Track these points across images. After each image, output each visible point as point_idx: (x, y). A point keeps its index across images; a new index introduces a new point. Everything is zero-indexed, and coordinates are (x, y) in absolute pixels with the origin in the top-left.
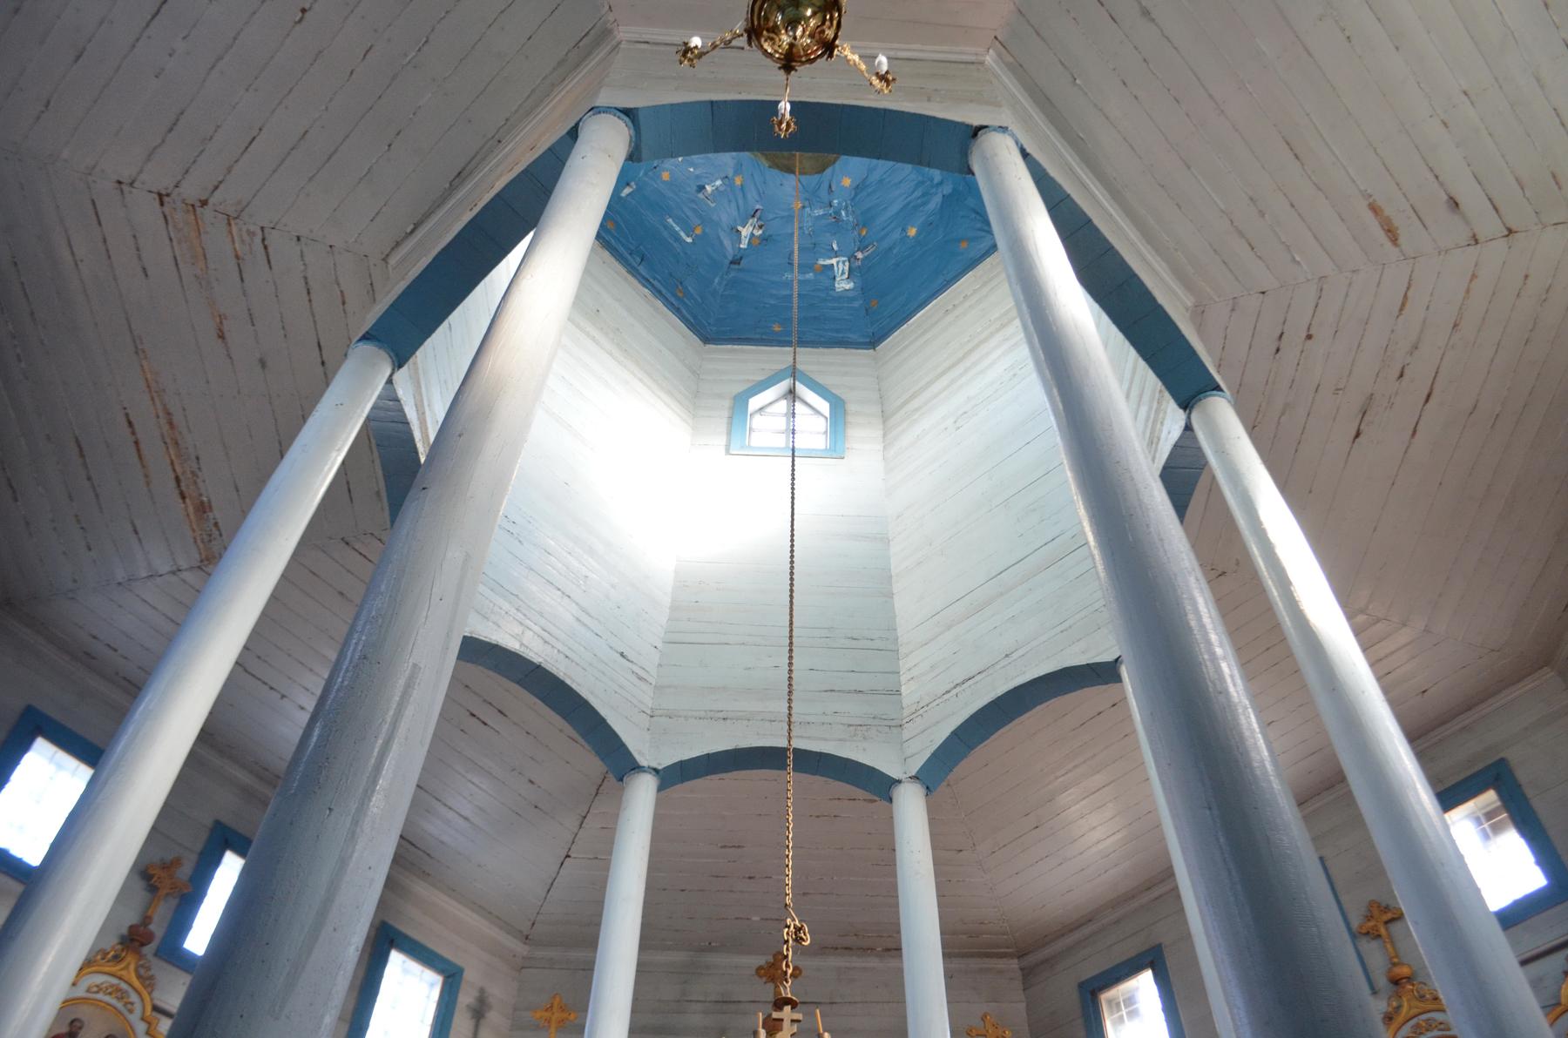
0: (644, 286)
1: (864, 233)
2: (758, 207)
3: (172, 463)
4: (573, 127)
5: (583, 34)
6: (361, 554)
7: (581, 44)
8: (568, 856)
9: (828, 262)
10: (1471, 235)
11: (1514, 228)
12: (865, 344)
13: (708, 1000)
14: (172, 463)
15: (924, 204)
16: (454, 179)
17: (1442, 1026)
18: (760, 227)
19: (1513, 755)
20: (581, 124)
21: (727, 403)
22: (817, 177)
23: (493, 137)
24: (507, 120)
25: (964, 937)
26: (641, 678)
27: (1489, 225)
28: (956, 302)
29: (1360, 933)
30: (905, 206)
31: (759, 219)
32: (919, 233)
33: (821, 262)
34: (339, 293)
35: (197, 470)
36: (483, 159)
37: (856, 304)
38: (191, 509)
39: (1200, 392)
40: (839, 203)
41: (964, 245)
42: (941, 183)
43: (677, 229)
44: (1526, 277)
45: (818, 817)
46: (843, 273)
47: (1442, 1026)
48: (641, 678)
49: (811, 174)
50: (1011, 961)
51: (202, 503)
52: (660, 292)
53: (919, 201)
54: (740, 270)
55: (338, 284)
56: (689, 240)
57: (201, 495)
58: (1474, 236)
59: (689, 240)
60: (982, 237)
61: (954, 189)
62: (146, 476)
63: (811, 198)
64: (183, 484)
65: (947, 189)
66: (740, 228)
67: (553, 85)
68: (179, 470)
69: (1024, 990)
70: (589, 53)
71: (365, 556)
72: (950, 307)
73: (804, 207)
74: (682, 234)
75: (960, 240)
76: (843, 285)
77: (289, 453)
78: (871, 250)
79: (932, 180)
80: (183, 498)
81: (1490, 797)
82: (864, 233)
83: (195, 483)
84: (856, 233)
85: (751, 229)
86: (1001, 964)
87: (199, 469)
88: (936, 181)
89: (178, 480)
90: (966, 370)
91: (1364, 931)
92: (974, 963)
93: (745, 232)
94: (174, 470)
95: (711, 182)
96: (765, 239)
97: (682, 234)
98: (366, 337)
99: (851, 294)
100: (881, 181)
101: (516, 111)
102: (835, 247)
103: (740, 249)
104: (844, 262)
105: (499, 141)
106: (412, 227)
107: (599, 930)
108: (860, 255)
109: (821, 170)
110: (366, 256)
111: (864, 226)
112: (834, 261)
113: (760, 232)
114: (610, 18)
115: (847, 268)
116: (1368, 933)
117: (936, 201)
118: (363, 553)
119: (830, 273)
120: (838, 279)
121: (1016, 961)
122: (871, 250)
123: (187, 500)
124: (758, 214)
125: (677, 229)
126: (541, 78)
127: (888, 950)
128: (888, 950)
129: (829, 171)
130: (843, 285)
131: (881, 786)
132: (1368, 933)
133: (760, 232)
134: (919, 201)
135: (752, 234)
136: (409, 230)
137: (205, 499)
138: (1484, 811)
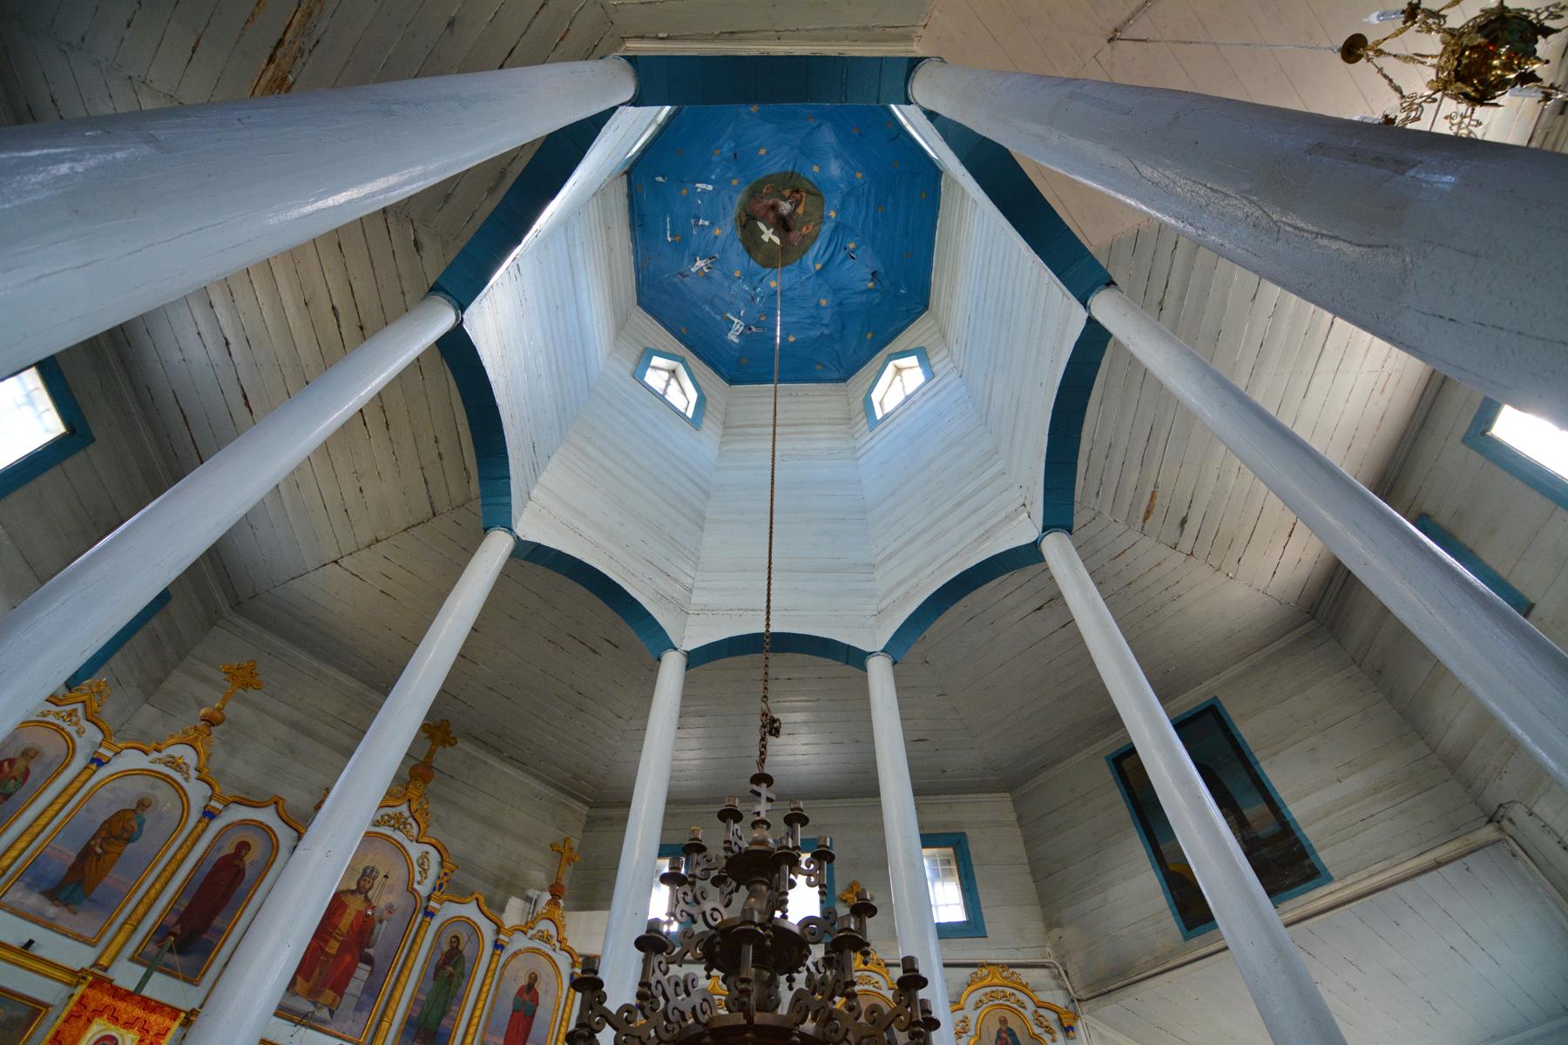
0: (632, 241)
2: (717, 255)
3: (289, 26)
4: (917, 58)
7: (888, 29)
8: (336, 562)
10: (1176, 542)
11: (1194, 554)
12: (726, 378)
13: (359, 727)
14: (289, 26)
15: (808, 329)
16: (724, 33)
17: (877, 985)
18: (709, 268)
19: (971, 834)
20: (927, 60)
21: (641, 348)
22: (760, 268)
23: (777, 31)
24: (798, 30)
25: (568, 775)
26: (534, 470)
27: (1186, 545)
28: (800, 394)
29: (841, 899)
31: (712, 263)
32: (794, 342)
33: (729, 315)
34: (565, 29)
36: (758, 39)
37: (733, 353)
41: (819, 367)
42: (826, 325)
43: (668, 227)
44: (1178, 582)
46: (737, 331)
47: (877, 985)
48: (534, 470)
49: (758, 263)
51: (285, 79)
52: (637, 253)
53: (807, 326)
55: (571, 23)
56: (669, 239)
57: (290, 72)
58: (1176, 544)
59: (669, 239)
60: (832, 370)
62: (253, 15)
63: (748, 276)
64: (281, 50)
65: (826, 331)
66: (698, 259)
67: (847, 38)
68: (289, 36)
69: (583, 832)
71: (389, 232)
72: (794, 394)
73: (739, 278)
74: (668, 233)
76: (733, 337)
77: (552, 65)
78: (761, 330)
80: (271, 59)
81: (950, 851)
82: (763, 319)
83: (295, 58)
85: (703, 264)
86: (576, 805)
87: (311, 51)
89: (280, 42)
90: (796, 433)
91: (844, 898)
92: (562, 798)
93: (700, 263)
94: (285, 32)
95: (705, 219)
96: (707, 276)
97: (668, 233)
98: (632, 60)
99: (734, 345)
100: (793, 299)
101: (808, 30)
102: (742, 313)
104: (741, 325)
105: (779, 39)
106: (666, 35)
110: (612, 23)
111: (765, 315)
112: (736, 320)
113: (707, 271)
114: (920, 32)
116: (846, 901)
117: (814, 333)
120: (732, 332)
121: (587, 808)
122: (761, 330)
123: (272, 66)
124: (714, 259)
125: (668, 227)
126: (844, 25)
127: (512, 758)
128: (512, 758)
129: (768, 270)
130: (733, 337)
131: (855, 658)
132: (846, 901)
133: (707, 271)
134: (807, 326)
135: (702, 268)
136: (661, 35)
137: (291, 78)
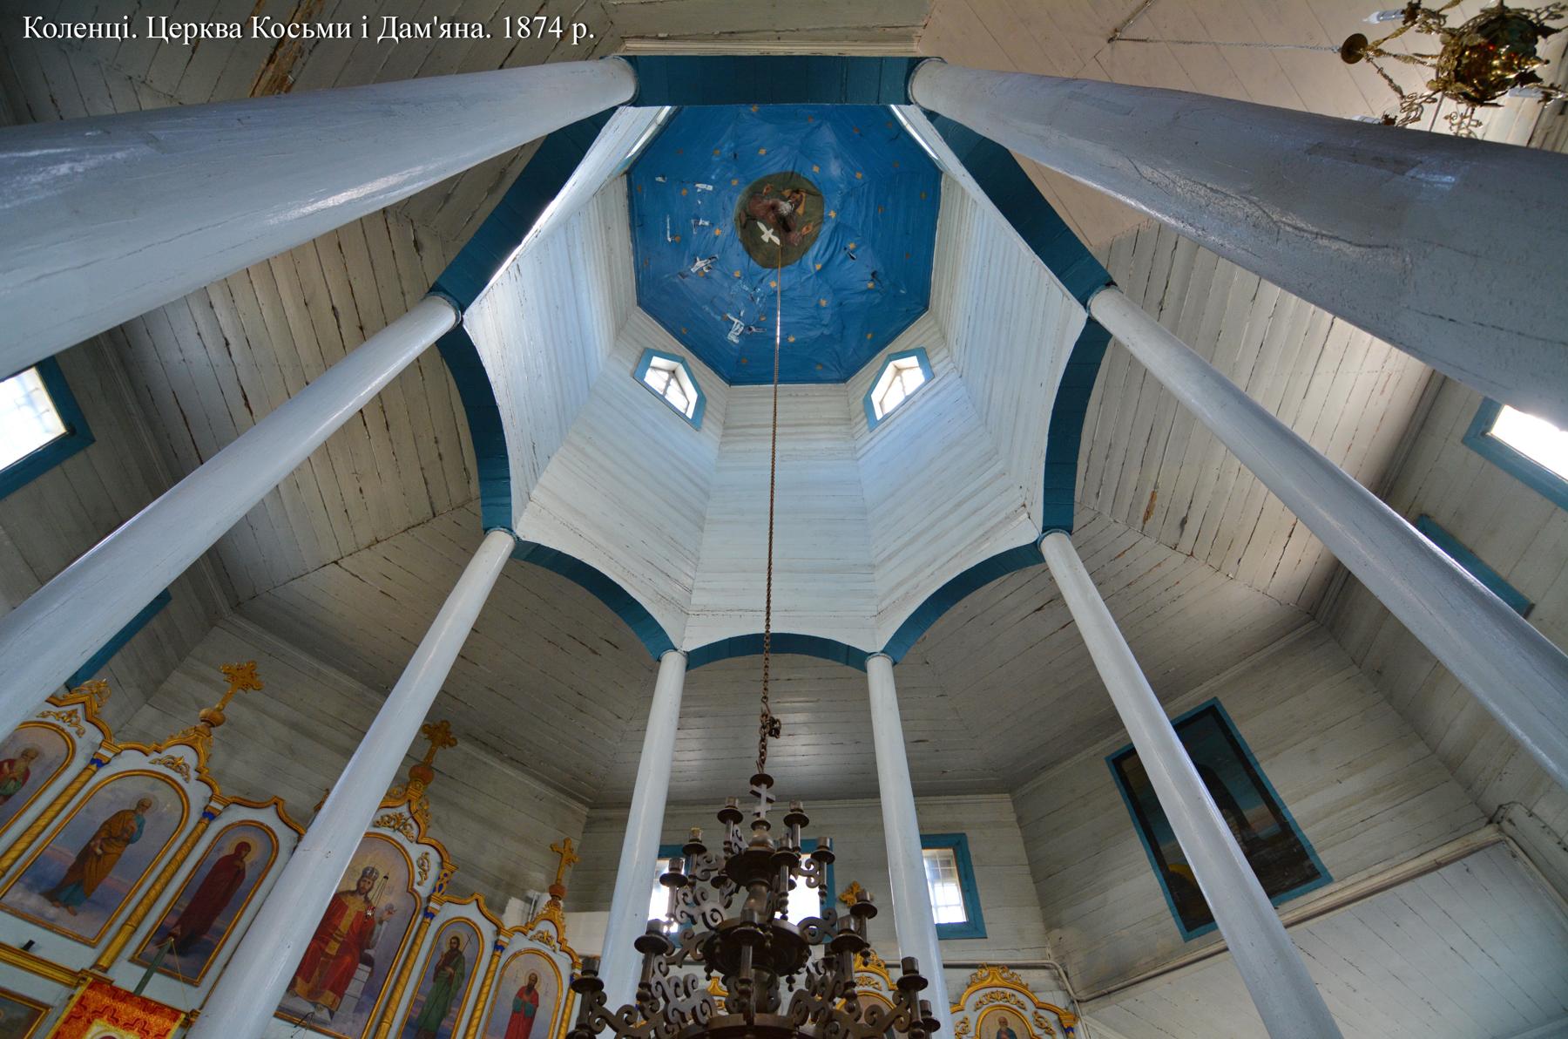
0: (632, 241)
1: (763, 319)
2: (717, 256)
5: (896, 25)
6: (388, 228)
7: (888, 29)
8: (336, 562)
9: (733, 319)
10: (1176, 542)
11: (1194, 554)
17: (877, 986)
18: (709, 268)
19: (972, 835)
23: (778, 31)
24: (798, 30)
26: (534, 470)
28: (800, 394)
30: (798, 323)
33: (729, 315)
35: (308, 51)
37: (733, 353)
38: (268, 75)
39: (1060, 527)
40: (760, 293)
41: (819, 368)
42: (826, 326)
43: (668, 227)
45: (549, 642)
46: (737, 331)
47: (877, 986)
48: (534, 470)
49: (758, 263)
50: (584, 808)
51: (285, 79)
52: (637, 253)
53: (807, 326)
54: (682, 281)
56: (669, 240)
57: (290, 72)
58: (1176, 545)
59: (669, 240)
61: (831, 335)
63: (748, 276)
64: (281, 50)
65: (826, 332)
66: (698, 259)
67: (847, 38)
69: (584, 833)
70: (887, 41)
73: (739, 278)
74: (668, 233)
75: (818, 363)
76: (733, 337)
78: (761, 331)
79: (821, 321)
80: (271, 60)
81: (950, 851)
84: (758, 315)
85: (703, 265)
86: (576, 805)
88: (823, 322)
91: (844, 899)
92: (562, 798)
93: (700, 264)
95: (705, 219)
96: (707, 276)
97: (668, 233)
98: (632, 60)
100: (792, 299)
101: (809, 30)
102: (742, 314)
103: (690, 270)
104: (741, 326)
105: (779, 39)
106: (666, 35)
107: (1085, 647)
108: (754, 330)
109: (765, 266)
110: (612, 23)
111: (765, 315)
112: (736, 321)
113: (707, 271)
115: (741, 330)
117: (815, 333)
118: (390, 229)
119: (730, 325)
120: (732, 332)
123: (272, 67)
124: (714, 260)
125: (668, 227)
126: (844, 25)
127: (512, 759)
128: (512, 759)
129: (768, 270)
130: (733, 337)
131: (855, 659)
132: (845, 902)
133: (707, 271)
134: (807, 326)
136: (661, 35)
138: (942, 859)
